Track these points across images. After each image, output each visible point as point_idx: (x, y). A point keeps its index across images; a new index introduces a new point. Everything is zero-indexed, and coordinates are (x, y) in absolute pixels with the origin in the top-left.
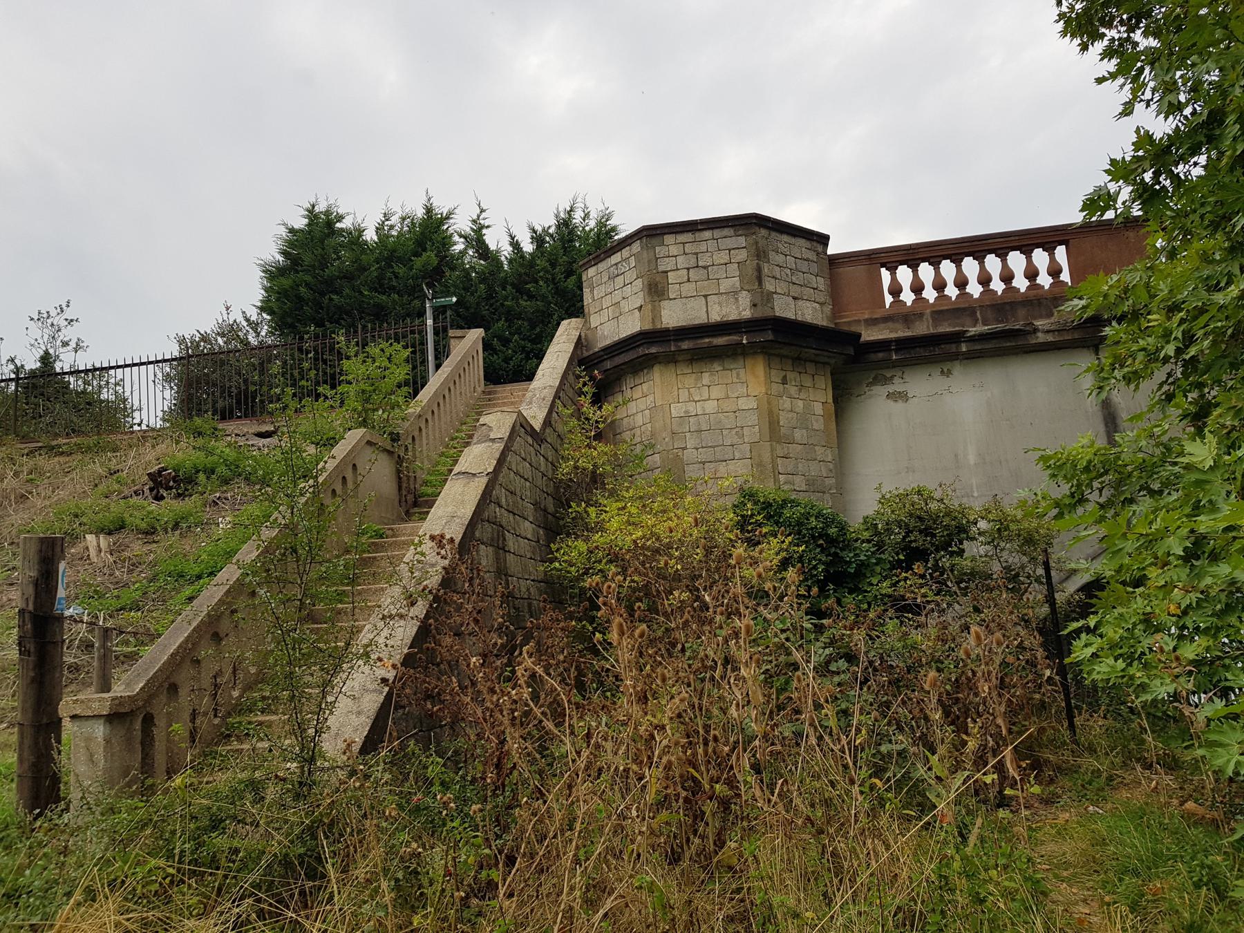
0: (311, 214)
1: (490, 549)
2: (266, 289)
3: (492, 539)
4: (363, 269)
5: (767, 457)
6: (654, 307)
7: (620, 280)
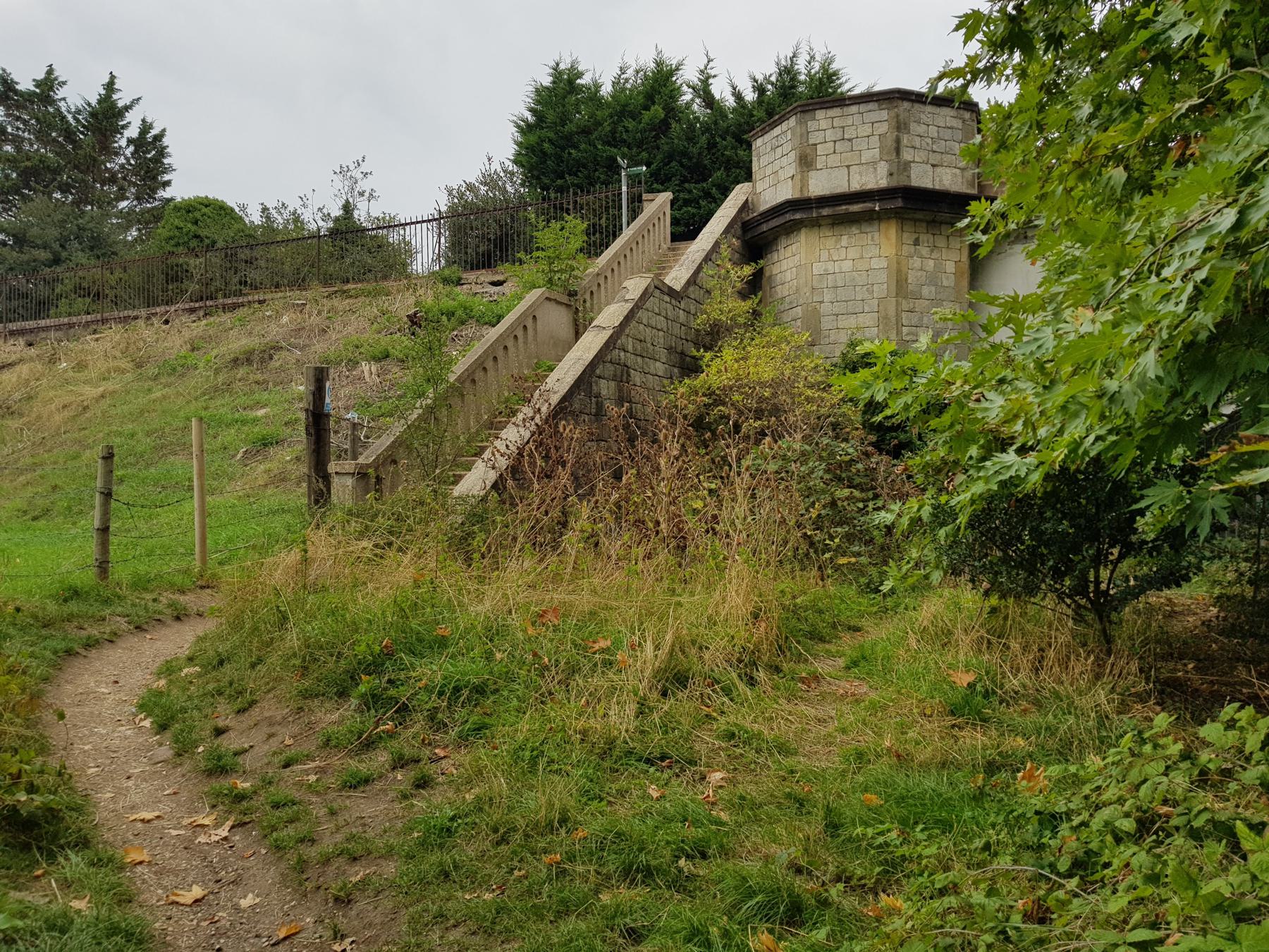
0: (557, 73)
1: (613, 384)
2: (519, 144)
3: (615, 376)
4: (599, 124)
5: (892, 312)
6: (802, 176)
7: (779, 150)
